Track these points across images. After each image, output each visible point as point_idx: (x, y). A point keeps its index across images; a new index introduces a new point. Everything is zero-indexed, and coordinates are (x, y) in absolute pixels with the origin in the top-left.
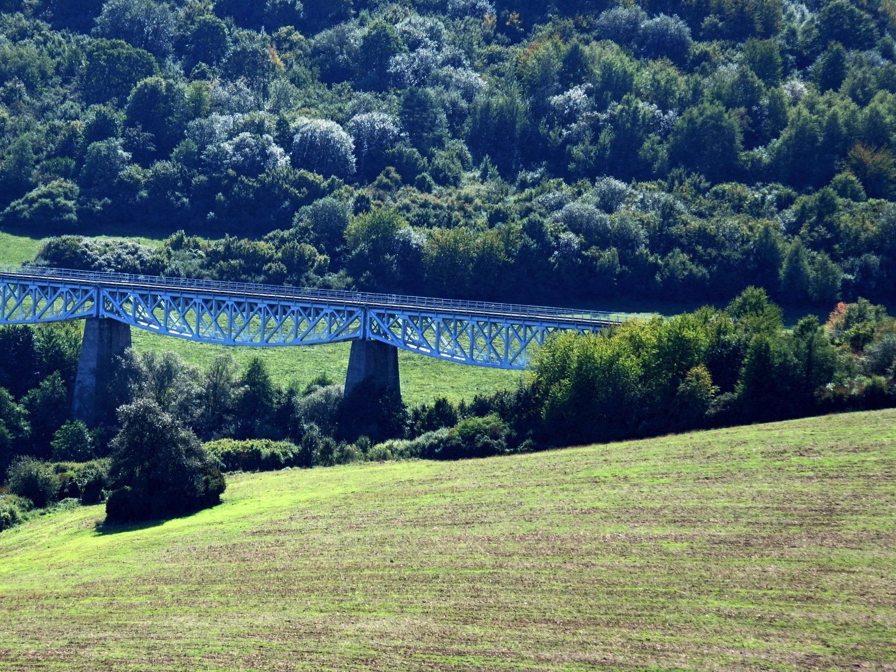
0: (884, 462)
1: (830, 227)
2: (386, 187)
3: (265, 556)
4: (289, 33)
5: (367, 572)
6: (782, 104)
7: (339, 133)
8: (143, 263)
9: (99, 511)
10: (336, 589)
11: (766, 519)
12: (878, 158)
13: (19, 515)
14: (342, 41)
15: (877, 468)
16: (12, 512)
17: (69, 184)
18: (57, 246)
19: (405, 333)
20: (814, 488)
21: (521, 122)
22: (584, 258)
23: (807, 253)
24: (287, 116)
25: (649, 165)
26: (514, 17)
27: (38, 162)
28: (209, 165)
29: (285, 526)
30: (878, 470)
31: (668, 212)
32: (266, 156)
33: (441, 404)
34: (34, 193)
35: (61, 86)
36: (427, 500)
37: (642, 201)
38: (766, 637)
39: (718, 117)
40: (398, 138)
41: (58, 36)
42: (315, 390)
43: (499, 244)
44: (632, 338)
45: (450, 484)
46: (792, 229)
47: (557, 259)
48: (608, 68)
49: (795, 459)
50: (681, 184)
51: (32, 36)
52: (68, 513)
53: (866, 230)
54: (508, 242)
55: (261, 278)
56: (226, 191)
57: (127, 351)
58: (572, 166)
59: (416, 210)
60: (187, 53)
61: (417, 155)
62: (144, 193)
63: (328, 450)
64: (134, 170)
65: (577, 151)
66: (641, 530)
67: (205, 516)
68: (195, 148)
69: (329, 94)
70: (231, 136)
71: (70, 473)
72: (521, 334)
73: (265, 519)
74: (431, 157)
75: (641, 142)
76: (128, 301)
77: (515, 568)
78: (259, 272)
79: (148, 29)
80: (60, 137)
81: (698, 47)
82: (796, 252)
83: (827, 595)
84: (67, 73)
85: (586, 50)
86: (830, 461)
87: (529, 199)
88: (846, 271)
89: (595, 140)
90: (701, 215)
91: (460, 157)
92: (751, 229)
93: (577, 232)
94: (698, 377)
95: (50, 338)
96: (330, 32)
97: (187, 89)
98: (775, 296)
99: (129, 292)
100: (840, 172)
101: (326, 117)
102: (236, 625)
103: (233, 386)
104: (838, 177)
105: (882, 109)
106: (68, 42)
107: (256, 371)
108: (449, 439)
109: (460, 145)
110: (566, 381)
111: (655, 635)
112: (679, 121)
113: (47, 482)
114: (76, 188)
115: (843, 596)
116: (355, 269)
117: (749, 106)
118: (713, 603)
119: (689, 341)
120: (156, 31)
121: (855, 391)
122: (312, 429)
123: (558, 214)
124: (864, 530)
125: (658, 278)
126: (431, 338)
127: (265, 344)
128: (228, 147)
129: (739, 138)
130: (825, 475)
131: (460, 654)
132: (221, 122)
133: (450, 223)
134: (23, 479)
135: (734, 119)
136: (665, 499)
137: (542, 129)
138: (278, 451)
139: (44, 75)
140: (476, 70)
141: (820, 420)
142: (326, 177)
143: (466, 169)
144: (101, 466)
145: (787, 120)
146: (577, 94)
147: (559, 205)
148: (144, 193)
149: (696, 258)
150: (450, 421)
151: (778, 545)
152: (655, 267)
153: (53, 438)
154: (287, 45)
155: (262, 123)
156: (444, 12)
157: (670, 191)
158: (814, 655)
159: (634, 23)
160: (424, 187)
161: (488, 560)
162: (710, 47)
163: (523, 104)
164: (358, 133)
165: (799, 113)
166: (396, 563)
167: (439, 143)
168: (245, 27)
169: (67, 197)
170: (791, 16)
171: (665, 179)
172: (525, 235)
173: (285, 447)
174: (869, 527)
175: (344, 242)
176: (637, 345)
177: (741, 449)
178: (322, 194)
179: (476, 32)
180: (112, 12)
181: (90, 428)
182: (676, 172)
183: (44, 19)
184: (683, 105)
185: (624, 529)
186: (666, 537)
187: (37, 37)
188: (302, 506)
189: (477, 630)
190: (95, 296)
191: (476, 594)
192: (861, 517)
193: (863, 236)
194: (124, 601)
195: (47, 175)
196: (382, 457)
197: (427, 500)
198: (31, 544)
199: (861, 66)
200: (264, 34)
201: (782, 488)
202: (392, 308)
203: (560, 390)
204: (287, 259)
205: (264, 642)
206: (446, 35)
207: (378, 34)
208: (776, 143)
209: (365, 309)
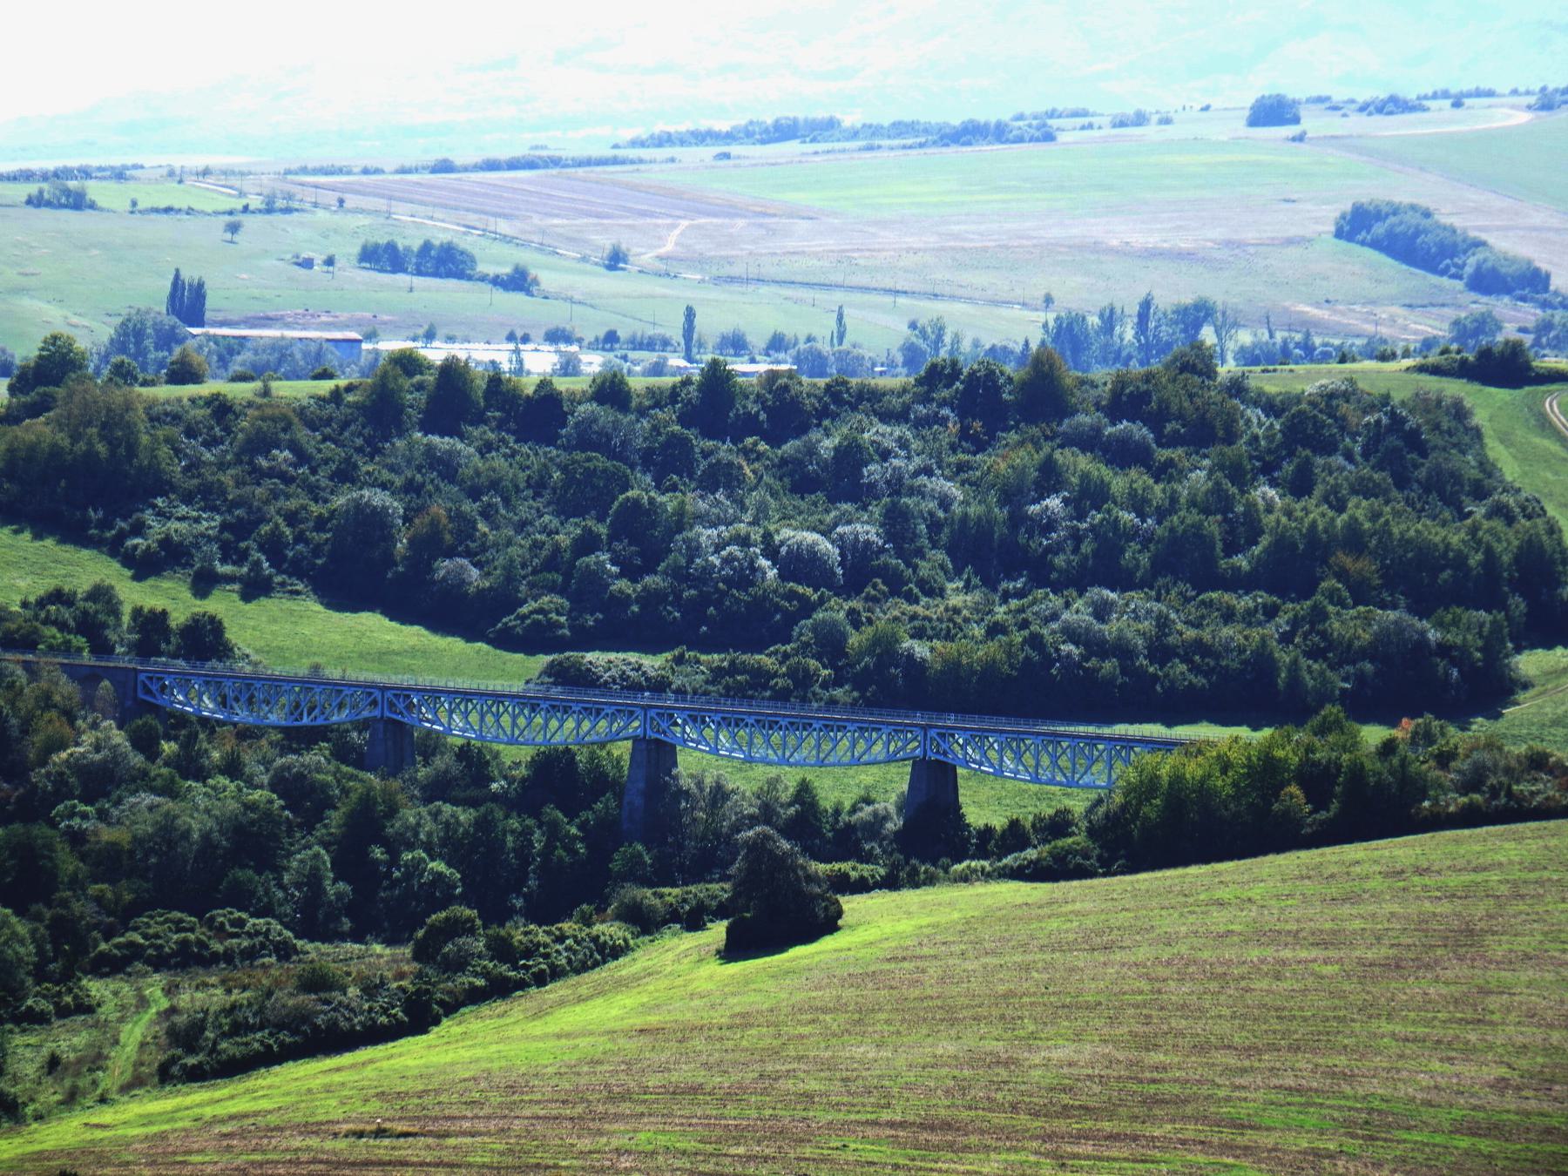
0: (1508, 881)
1: (1324, 635)
2: (875, 600)
3: (915, 983)
4: (755, 444)
6: (1257, 511)
7: (825, 546)
8: (647, 679)
10: (1002, 1017)
11: (1410, 941)
12: (1359, 565)
14: (811, 451)
15: (1502, 887)
16: (625, 940)
17: (558, 600)
18: (560, 663)
20: (1444, 908)
21: (999, 532)
22: (1086, 670)
23: (1304, 662)
24: (772, 528)
25: (1131, 574)
26: (977, 425)
27: (524, 577)
28: (696, 579)
29: (918, 951)
30: (1504, 889)
31: (1163, 623)
32: (754, 569)
34: (524, 610)
35: (534, 499)
36: (1054, 924)
37: (1134, 611)
38: (1450, 1060)
39: (1198, 526)
40: (882, 550)
41: (525, 449)
42: (861, 809)
43: (1001, 656)
44: (1219, 757)
45: (1070, 907)
46: (1286, 639)
47: (1059, 670)
48: (1085, 476)
49: (1416, 879)
50: (1168, 592)
51: (497, 450)
53: (1359, 638)
54: (1009, 655)
55: (768, 694)
56: (718, 604)
57: (674, 772)
58: (1054, 575)
60: (655, 465)
61: (902, 566)
62: (635, 608)
64: (622, 585)
65: (1059, 560)
66: (1287, 954)
67: (827, 943)
68: (683, 562)
69: (803, 505)
70: (718, 548)
71: (668, 899)
72: (462, 707)
74: (915, 568)
75: (1122, 551)
76: (676, 724)
77: (1177, 992)
78: (765, 687)
79: (616, 441)
80: (544, 553)
81: (1163, 454)
82: (1295, 662)
83: (1496, 1017)
84: (538, 486)
86: (1454, 881)
88: (1345, 679)
89: (1076, 550)
91: (942, 567)
92: (1246, 638)
93: (1077, 644)
94: (1292, 796)
96: (797, 442)
97: (668, 502)
100: (1323, 579)
101: (814, 529)
102: (923, 1054)
103: (782, 806)
104: (1324, 585)
105: (1360, 514)
106: (536, 454)
107: (804, 788)
108: (1038, 860)
109: (940, 556)
110: (1158, 802)
111: (1341, 1061)
112: (1160, 531)
113: (652, 909)
114: (567, 604)
115: (1512, 1017)
116: (860, 682)
117: (1224, 513)
118: (1387, 1028)
119: (1280, 760)
120: (623, 443)
121: (1452, 809)
123: (1055, 626)
124: (1511, 951)
125: (1158, 688)
126: (993, 755)
127: (821, 763)
128: (715, 560)
129: (1219, 545)
130: (1454, 896)
131: (1154, 1081)
134: (627, 906)
135: (1213, 526)
136: (1298, 921)
137: (1022, 539)
138: (866, 874)
139: (518, 490)
140: (948, 479)
142: (815, 591)
143: (951, 580)
144: (720, 890)
145: (1460, 551)
146: (1054, 503)
147: (1054, 617)
148: (635, 608)
149: (1195, 669)
151: (1428, 967)
152: (1155, 678)
153: (611, 860)
154: (754, 456)
155: (748, 536)
156: (907, 421)
157: (1158, 600)
158: (1503, 1079)
159: (1097, 430)
161: (1144, 985)
162: (1176, 453)
163: (1001, 514)
164: (841, 542)
165: (1278, 522)
166: (1051, 989)
167: (920, 553)
168: (711, 438)
169: (558, 613)
170: (1248, 421)
171: (1151, 588)
172: (1027, 647)
174: (1515, 947)
175: (846, 655)
177: (1358, 869)
179: (945, 440)
180: (577, 424)
181: (649, 850)
182: (1161, 581)
183: (508, 431)
184: (1161, 515)
185: (1269, 952)
186: (1315, 960)
187: (504, 450)
189: (1162, 1057)
192: (1504, 938)
193: (1357, 643)
195: (535, 591)
196: (965, 878)
197: (1054, 924)
198: (658, 973)
199: (1330, 474)
200: (728, 444)
201: (1413, 909)
202: (669, 708)
203: (1152, 810)
204: (792, 674)
205: (956, 1073)
206: (916, 445)
207: (850, 445)
208: (1257, 550)
209: (925, 728)
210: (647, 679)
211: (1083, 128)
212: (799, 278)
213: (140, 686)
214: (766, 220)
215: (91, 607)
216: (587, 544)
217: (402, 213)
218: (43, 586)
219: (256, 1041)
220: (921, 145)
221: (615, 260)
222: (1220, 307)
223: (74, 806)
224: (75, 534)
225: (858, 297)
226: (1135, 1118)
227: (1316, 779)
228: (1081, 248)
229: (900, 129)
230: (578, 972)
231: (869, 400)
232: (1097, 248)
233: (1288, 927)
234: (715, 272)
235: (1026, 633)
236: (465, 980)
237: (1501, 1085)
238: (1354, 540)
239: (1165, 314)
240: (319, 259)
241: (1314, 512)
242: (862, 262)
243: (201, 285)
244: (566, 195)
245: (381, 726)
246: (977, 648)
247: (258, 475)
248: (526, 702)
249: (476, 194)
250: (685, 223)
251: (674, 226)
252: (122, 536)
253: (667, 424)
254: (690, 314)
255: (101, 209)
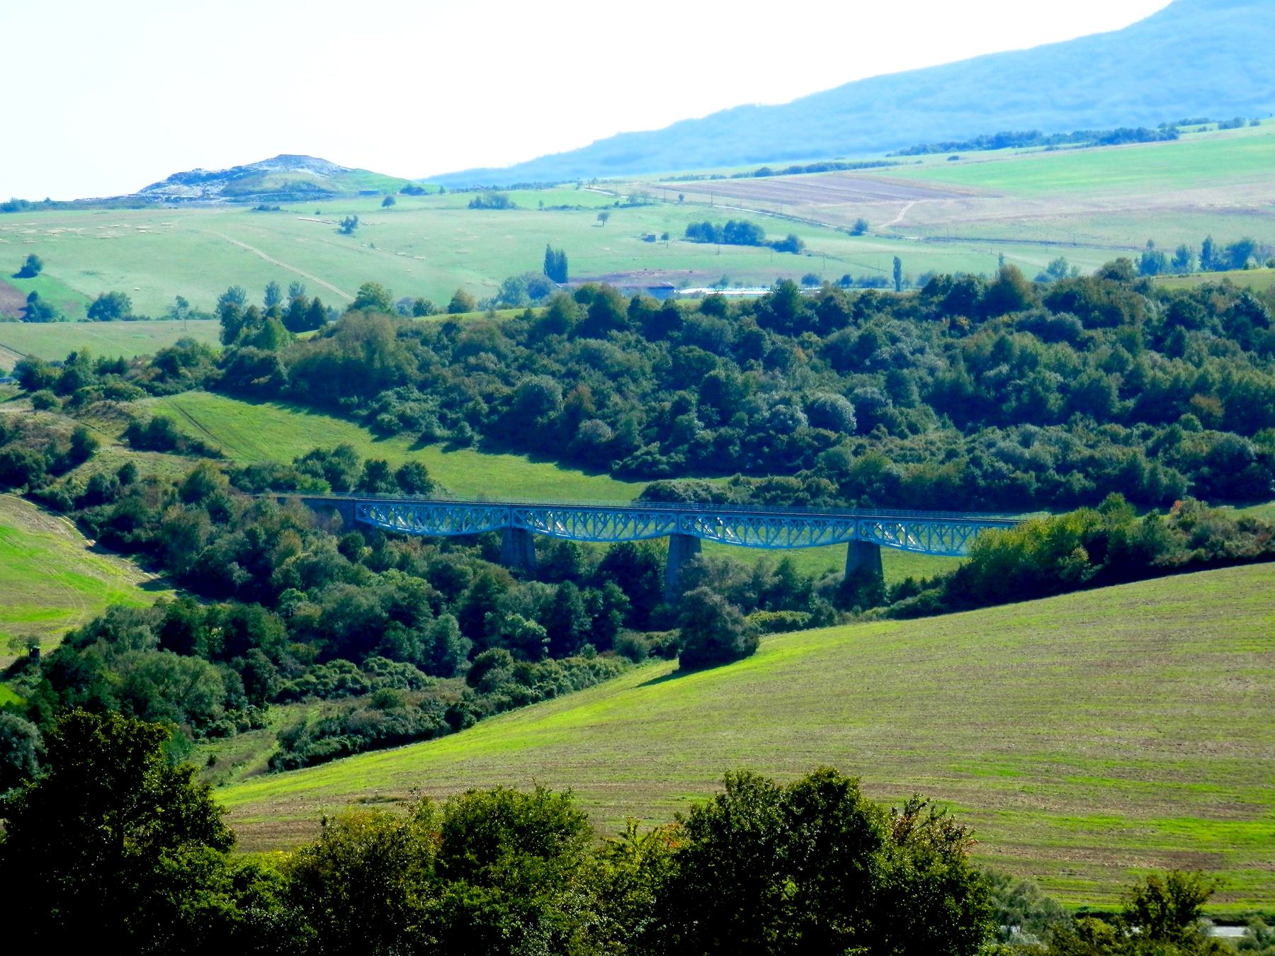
5: (852, 696)
9: (674, 664)
11: (1123, 649)
13: (621, 669)
18: (653, 487)
19: (884, 534)
29: (799, 668)
31: (1066, 447)
33: (909, 581)
34: (638, 453)
38: (1119, 728)
45: (911, 634)
49: (1142, 607)
52: (655, 667)
59: (897, 451)
63: (830, 617)
72: (938, 531)
73: (785, 663)
76: (719, 524)
85: (1010, 338)
86: (1166, 607)
87: (974, 441)
90: (1091, 447)
92: (1124, 454)
93: (1006, 462)
95: (646, 550)
97: (739, 377)
98: (1130, 498)
99: (698, 516)
105: (1210, 369)
111: (1043, 730)
122: (817, 601)
129: (1115, 393)
130: (1163, 617)
132: (761, 399)
133: (920, 460)
141: (1162, 581)
149: (1087, 476)
150: (914, 592)
160: (903, 436)
161: (934, 684)
173: (801, 616)
176: (1036, 535)
177: (1107, 602)
178: (834, 444)
188: (811, 654)
190: (675, 519)
191: (924, 707)
194: (688, 723)
196: (870, 619)
204: (808, 489)
210: (712, 496)
211: (1200, 130)
212: (984, 236)
213: (357, 511)
214: (968, 199)
215: (335, 460)
216: (681, 407)
217: (720, 201)
218: (307, 448)
219: (334, 743)
220: (1087, 146)
221: (859, 230)
222: (1258, 242)
223: (293, 592)
224: (341, 412)
225: (1009, 246)
226: (889, 773)
227: (1096, 544)
228: (1179, 209)
229: (1078, 137)
230: (576, 689)
231: (890, 305)
232: (1190, 209)
233: (1045, 643)
234: (928, 234)
235: (971, 455)
236: (497, 696)
237: (1148, 743)
238: (1202, 386)
239: (1221, 250)
240: (658, 236)
241: (1180, 369)
242: (1028, 224)
243: (563, 256)
244: (836, 188)
245: (510, 533)
246: (932, 470)
247: (470, 369)
248: (626, 513)
249: (774, 189)
250: (911, 203)
251: (904, 205)
252: (375, 413)
253: (749, 325)
254: (897, 263)
255: (519, 209)
